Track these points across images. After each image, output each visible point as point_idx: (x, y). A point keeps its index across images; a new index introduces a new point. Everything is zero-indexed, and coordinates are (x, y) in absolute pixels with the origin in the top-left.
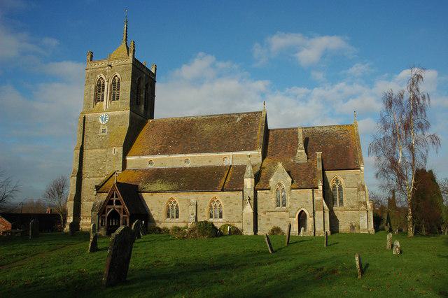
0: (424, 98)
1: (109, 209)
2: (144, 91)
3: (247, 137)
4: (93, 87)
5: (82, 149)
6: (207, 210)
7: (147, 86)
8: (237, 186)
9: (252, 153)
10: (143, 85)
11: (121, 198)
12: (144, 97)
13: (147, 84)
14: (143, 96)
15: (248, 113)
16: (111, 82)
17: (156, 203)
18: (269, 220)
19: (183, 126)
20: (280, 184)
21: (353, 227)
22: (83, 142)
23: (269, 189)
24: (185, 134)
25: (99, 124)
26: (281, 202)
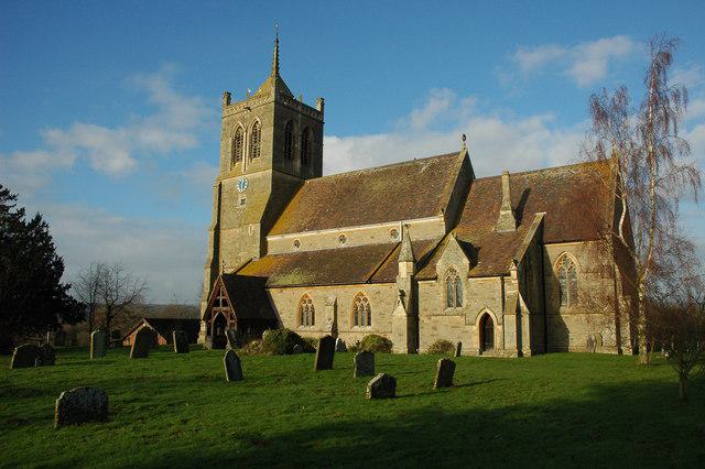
0: (676, 96)
1: (215, 312)
2: (300, 139)
3: (429, 195)
4: (230, 142)
5: (217, 229)
6: (350, 312)
7: (306, 131)
8: (390, 276)
9: (432, 220)
10: (297, 130)
11: (227, 297)
12: (299, 148)
13: (307, 128)
14: (298, 146)
15: (439, 157)
16: (250, 131)
17: (286, 303)
18: (435, 328)
19: (346, 186)
20: (452, 270)
21: (590, 343)
22: (219, 220)
23: (436, 278)
24: (353, 199)
25: (237, 193)
26: (453, 299)
